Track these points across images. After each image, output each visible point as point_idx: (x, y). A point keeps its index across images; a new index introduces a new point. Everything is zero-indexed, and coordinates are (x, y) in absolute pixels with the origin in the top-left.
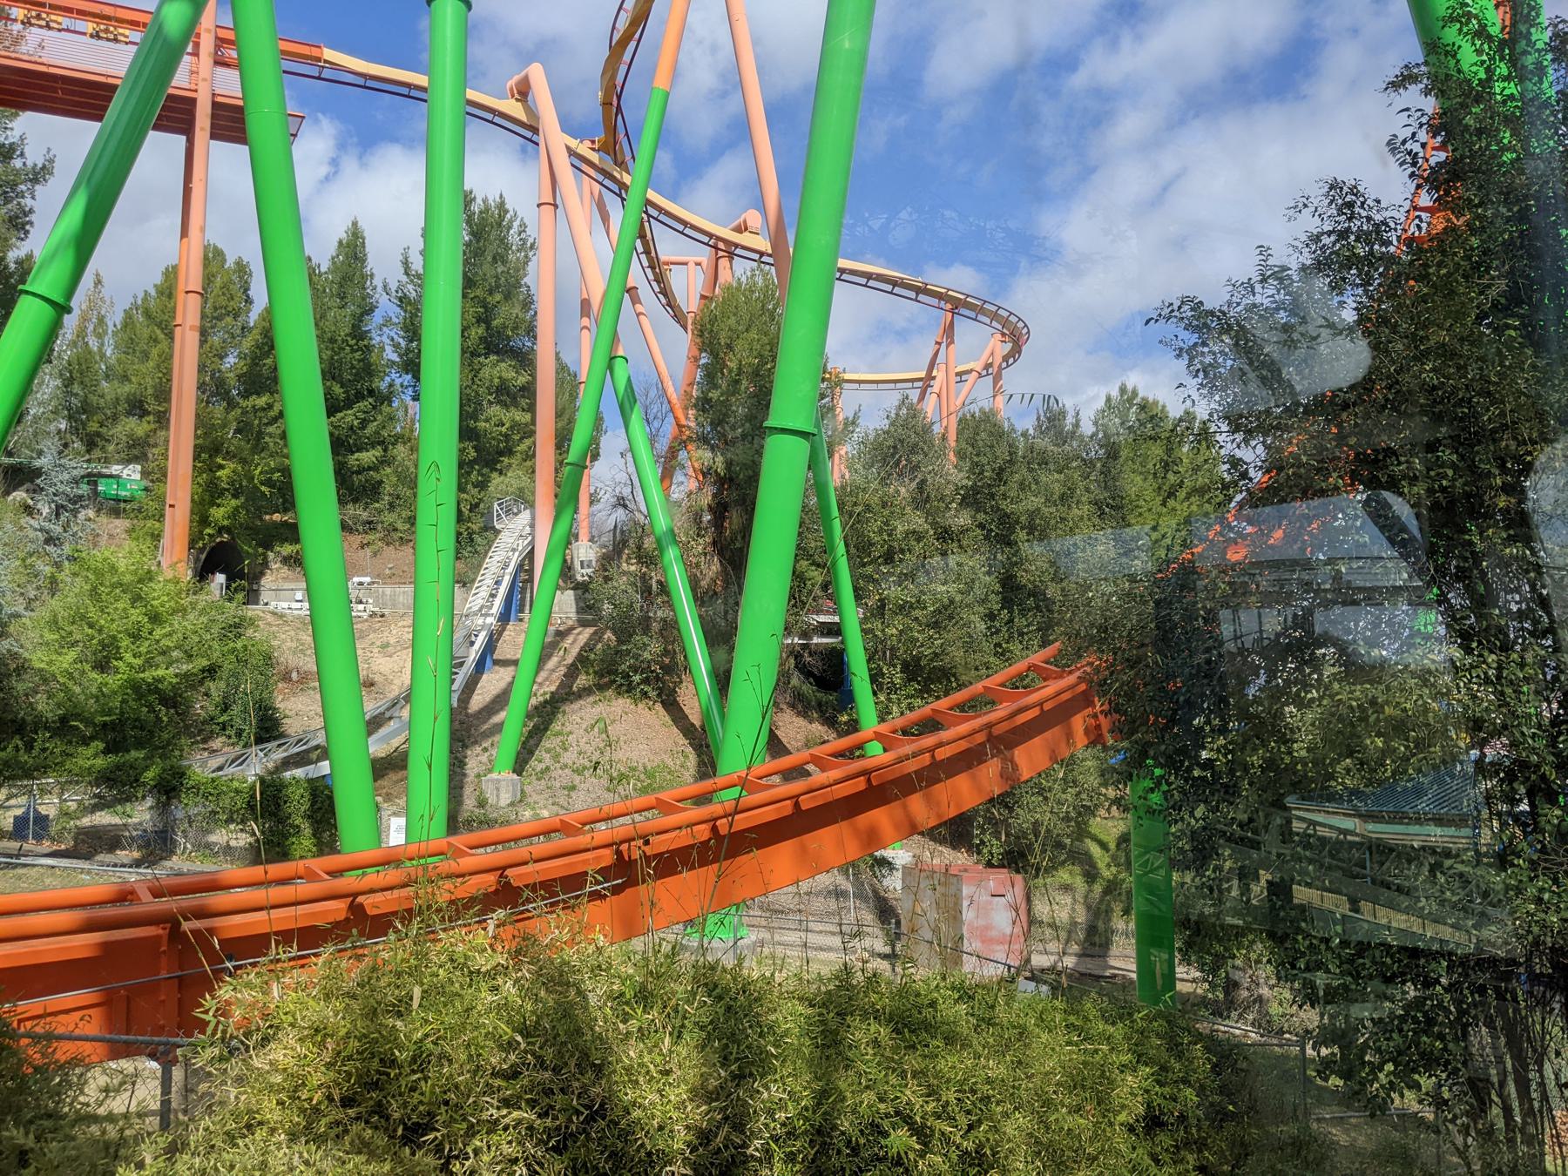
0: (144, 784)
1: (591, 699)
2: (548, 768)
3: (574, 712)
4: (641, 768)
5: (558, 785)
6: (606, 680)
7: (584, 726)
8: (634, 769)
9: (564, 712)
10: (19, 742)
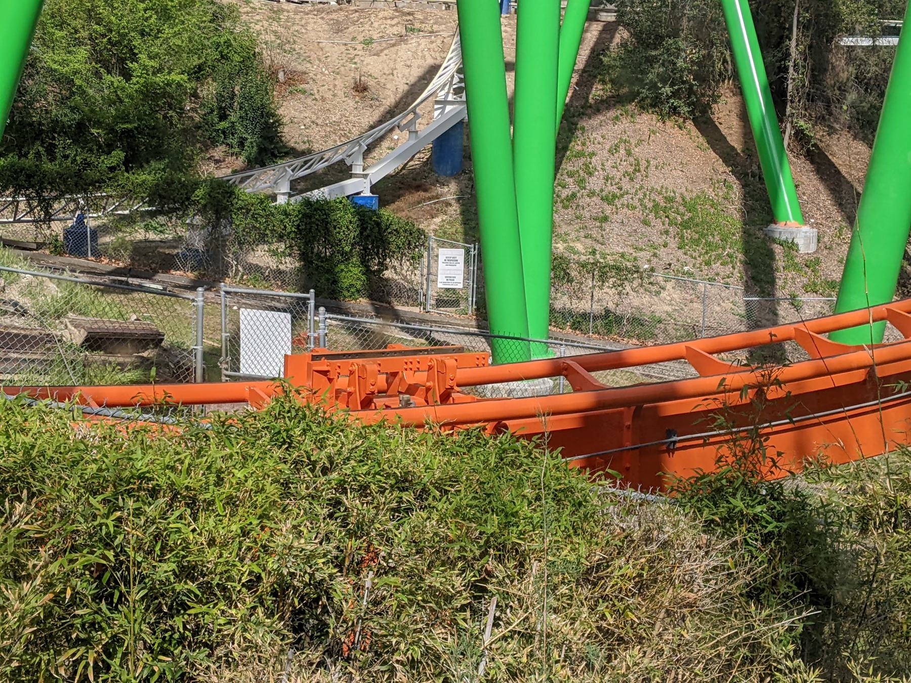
0: (195, 203)
1: (612, 114)
2: (574, 195)
3: (594, 129)
4: (679, 199)
5: (588, 215)
6: (625, 90)
7: (607, 147)
8: (669, 200)
9: (583, 128)
10: (41, 149)
